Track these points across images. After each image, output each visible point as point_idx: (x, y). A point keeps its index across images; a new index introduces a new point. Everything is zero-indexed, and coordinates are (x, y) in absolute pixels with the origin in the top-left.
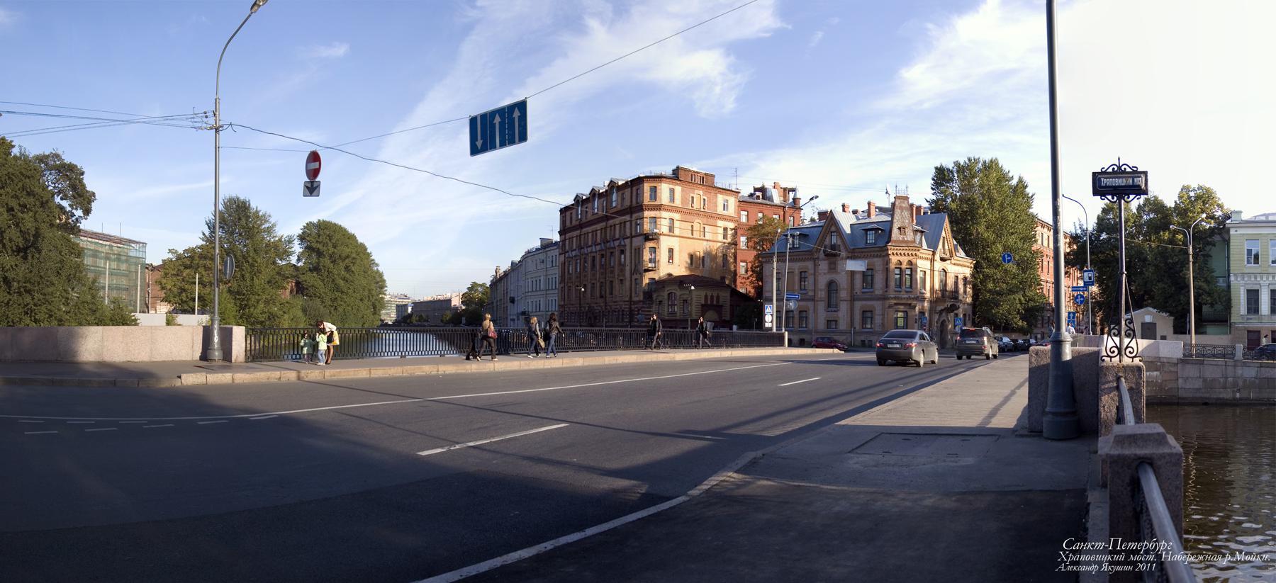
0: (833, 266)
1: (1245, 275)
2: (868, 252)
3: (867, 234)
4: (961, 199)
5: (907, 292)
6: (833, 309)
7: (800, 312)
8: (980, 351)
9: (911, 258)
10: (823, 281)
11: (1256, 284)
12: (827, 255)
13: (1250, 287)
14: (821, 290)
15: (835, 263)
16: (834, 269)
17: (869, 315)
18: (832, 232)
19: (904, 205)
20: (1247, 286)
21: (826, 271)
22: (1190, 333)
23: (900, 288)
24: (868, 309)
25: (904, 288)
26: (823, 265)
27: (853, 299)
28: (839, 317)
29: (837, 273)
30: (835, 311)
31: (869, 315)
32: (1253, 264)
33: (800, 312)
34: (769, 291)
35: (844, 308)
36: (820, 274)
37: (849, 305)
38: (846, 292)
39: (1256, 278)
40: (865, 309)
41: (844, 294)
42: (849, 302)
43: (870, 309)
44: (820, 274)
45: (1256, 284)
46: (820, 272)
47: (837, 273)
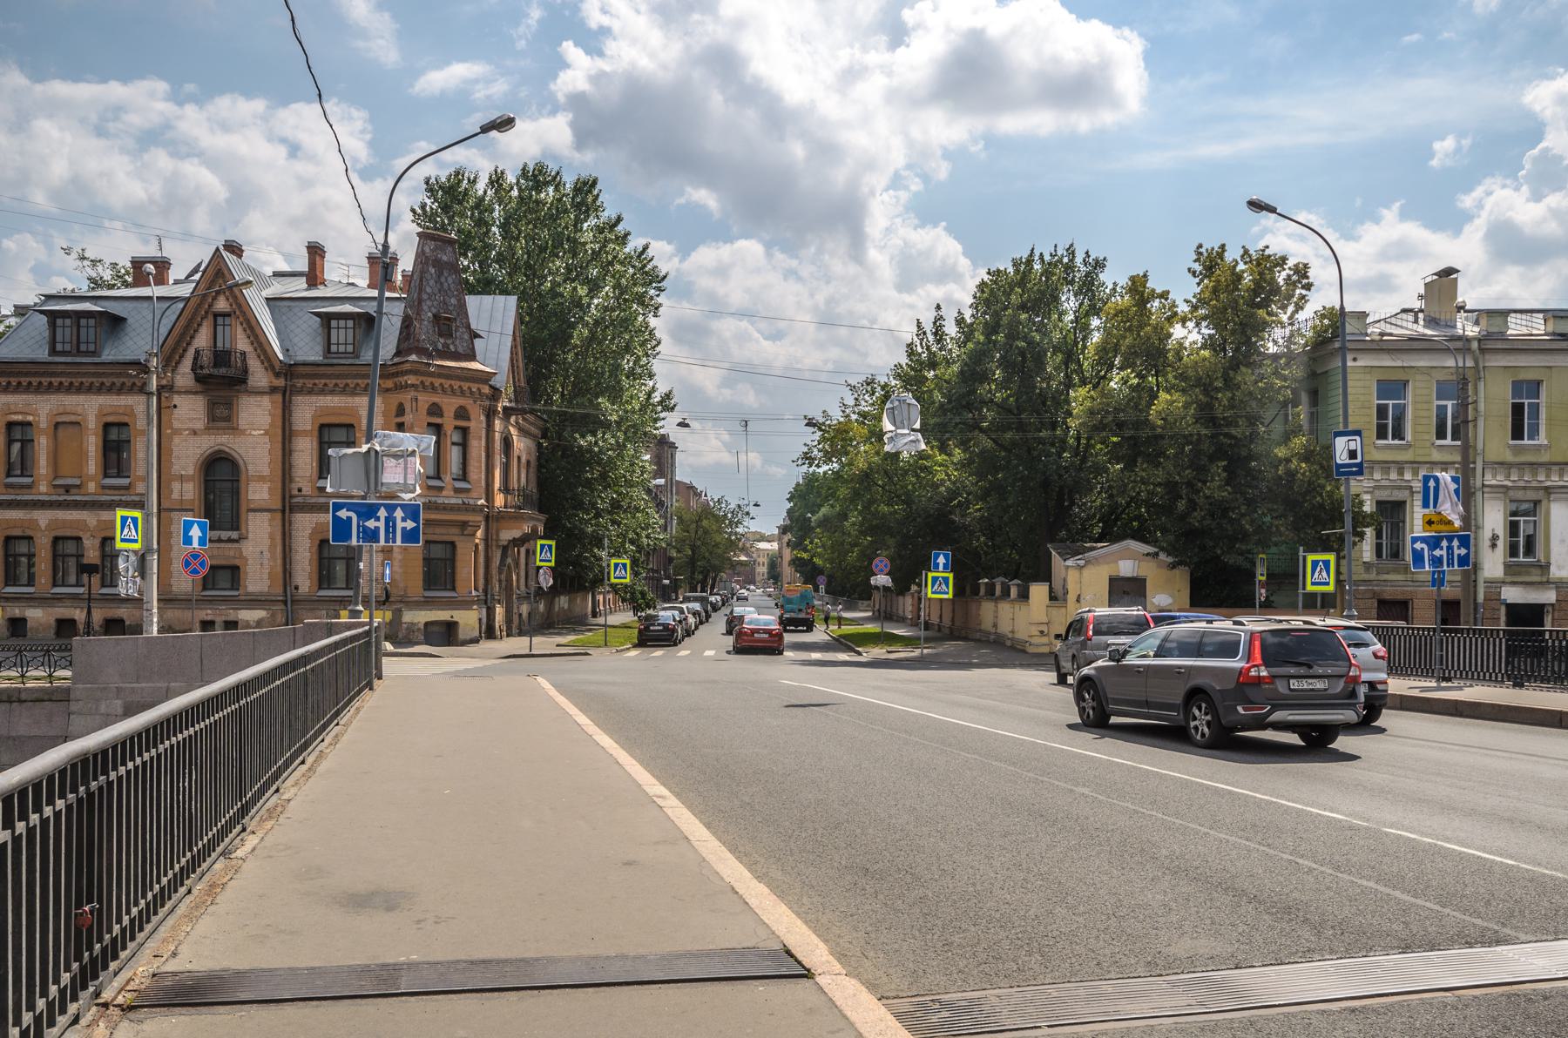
0: (220, 411)
1: (1376, 466)
2: (339, 376)
3: (329, 328)
4: (832, 546)
5: (457, 491)
6: (225, 535)
7: (56, 540)
8: (1558, 74)
9: (436, 399)
10: (188, 453)
11: (1400, 488)
12: (204, 381)
13: (1384, 495)
14: (182, 478)
15: (229, 405)
16: (228, 419)
17: (22, 548)
18: (216, 315)
19: (445, 258)
20: (1377, 493)
21: (199, 425)
22: (1112, 603)
23: (438, 477)
24: (68, 533)
25: (447, 478)
26: (190, 410)
27: (288, 506)
28: (241, 556)
29: (235, 430)
30: (230, 540)
31: (70, 548)
32: (1526, 402)
33: (56, 540)
34: (1433, 575)
35: (260, 532)
36: (177, 432)
37: (278, 522)
38: (266, 487)
39: (1401, 473)
40: (60, 533)
41: (259, 492)
42: (279, 515)
43: (75, 534)
44: (177, 432)
45: (1400, 488)
46: (176, 425)
47: (235, 430)
